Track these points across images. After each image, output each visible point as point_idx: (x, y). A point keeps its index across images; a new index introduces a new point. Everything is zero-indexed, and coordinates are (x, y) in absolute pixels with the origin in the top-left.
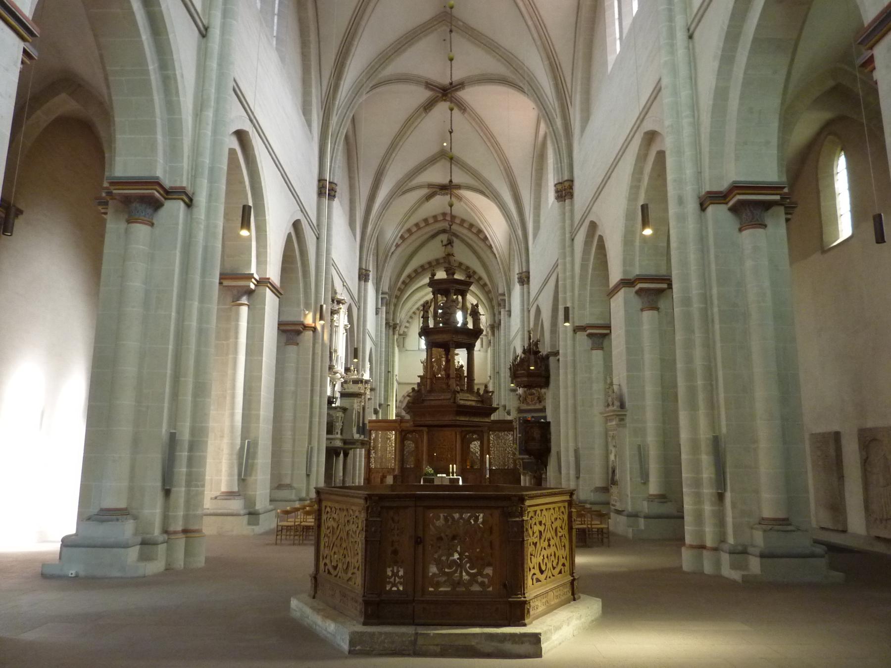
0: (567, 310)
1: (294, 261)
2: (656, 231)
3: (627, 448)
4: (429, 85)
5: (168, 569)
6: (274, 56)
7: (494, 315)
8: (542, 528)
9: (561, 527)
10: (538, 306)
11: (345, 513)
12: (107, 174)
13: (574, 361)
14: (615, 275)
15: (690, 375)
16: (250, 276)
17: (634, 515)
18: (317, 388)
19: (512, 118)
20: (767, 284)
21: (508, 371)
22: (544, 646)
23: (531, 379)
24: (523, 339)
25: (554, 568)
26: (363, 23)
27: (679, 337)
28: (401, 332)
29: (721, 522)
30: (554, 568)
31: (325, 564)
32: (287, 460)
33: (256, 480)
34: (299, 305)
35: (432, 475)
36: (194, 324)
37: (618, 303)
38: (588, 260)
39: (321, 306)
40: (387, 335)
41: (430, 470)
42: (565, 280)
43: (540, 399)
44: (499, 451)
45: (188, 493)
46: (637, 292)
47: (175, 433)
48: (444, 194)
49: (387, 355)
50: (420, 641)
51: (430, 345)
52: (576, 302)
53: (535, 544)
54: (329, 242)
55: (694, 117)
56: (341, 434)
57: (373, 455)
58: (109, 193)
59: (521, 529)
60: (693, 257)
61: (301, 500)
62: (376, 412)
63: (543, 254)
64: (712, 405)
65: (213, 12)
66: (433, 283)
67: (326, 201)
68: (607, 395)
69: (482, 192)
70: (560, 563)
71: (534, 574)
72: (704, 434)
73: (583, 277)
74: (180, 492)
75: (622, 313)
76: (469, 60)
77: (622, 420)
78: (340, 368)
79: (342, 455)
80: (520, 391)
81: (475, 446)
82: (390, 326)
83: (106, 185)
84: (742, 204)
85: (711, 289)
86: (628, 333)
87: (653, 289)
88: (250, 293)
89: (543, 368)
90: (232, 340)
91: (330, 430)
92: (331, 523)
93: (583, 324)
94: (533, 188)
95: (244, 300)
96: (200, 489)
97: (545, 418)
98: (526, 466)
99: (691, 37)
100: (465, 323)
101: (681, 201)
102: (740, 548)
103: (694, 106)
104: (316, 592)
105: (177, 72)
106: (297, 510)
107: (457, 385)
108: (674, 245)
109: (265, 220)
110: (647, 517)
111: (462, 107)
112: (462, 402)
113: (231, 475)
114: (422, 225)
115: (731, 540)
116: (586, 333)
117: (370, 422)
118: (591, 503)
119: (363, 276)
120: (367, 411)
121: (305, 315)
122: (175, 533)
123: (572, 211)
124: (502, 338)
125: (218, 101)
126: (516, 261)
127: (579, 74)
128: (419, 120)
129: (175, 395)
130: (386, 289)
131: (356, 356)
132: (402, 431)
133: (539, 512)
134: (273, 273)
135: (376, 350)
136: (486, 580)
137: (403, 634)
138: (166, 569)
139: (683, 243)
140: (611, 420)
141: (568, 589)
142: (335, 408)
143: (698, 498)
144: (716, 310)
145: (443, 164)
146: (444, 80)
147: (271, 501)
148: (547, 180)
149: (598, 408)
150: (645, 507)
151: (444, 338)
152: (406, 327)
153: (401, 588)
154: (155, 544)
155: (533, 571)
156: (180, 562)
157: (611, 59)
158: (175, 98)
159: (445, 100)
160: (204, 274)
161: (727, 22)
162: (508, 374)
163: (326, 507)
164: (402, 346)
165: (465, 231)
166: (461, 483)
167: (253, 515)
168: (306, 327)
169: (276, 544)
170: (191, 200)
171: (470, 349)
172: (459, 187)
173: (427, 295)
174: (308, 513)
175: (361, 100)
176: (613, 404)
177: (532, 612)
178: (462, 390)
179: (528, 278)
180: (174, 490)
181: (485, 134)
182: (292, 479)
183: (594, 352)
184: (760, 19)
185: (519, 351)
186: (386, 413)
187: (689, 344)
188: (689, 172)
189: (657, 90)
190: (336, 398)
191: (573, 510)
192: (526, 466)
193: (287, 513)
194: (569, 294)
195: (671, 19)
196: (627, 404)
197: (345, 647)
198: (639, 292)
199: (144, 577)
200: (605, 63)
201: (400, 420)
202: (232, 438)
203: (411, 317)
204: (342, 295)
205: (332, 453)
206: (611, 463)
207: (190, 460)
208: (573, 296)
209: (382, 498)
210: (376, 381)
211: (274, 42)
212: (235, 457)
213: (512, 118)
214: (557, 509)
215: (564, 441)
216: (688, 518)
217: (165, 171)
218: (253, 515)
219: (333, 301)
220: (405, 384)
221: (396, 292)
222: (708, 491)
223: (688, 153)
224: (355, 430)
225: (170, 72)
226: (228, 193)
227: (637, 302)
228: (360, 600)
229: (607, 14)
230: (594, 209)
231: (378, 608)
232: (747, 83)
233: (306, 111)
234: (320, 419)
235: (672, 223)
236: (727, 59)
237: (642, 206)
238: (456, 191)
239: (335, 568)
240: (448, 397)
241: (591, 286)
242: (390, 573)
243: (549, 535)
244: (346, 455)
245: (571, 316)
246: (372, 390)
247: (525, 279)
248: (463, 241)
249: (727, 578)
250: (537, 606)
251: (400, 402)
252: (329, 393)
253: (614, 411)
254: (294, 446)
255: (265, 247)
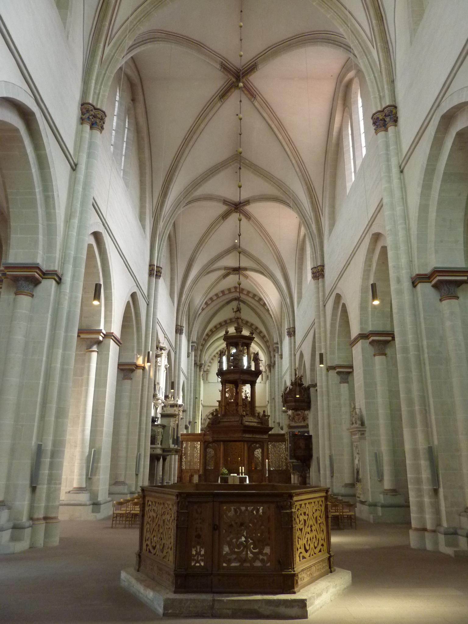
0: (321, 355)
1: (131, 320)
2: (382, 301)
3: (367, 453)
4: (225, 202)
5: (32, 547)
6: (121, 183)
7: (271, 357)
8: (306, 518)
9: (320, 517)
10: (301, 352)
11: (162, 506)
12: (3, 261)
13: (328, 392)
14: (355, 331)
15: (410, 403)
16: (99, 332)
17: (374, 505)
18: (145, 411)
19: (282, 224)
20: (461, 337)
21: (281, 398)
22: (310, 609)
23: (297, 404)
24: (291, 375)
25: (315, 548)
26: (182, 161)
27: (401, 375)
28: (205, 370)
29: (437, 512)
30: (315, 548)
31: (147, 545)
32: (122, 463)
33: (99, 479)
34: (133, 351)
35: (227, 474)
36: (59, 365)
37: (358, 350)
38: (336, 320)
39: (149, 353)
40: (195, 372)
41: (225, 471)
42: (320, 333)
43: (305, 419)
44: (276, 457)
45: (49, 489)
46: (370, 343)
47: (41, 445)
48: (236, 274)
49: (195, 386)
50: (217, 606)
51: (223, 383)
52: (328, 350)
53: (301, 530)
54: (155, 302)
55: (406, 224)
56: (161, 444)
57: (184, 460)
58: (4, 274)
59: (290, 518)
60: (409, 319)
61: (132, 493)
62: (186, 428)
63: (305, 315)
64: (426, 424)
65: (81, 154)
66: (227, 338)
67: (154, 279)
68: (351, 416)
69: (262, 273)
70: (320, 544)
71: (301, 553)
72: (422, 446)
73: (332, 332)
74: (43, 489)
75: (360, 357)
76: (252, 185)
77: (363, 434)
78: (161, 396)
79: (161, 459)
80: (290, 412)
81: (258, 453)
82: (197, 366)
83: (2, 268)
84: (441, 282)
85: (422, 341)
86: (365, 372)
87: (381, 341)
88: (99, 343)
89: (306, 396)
90: (85, 376)
91: (153, 442)
92: (152, 514)
93: (428, 270)
94: (296, 281)
95: (95, 348)
96: (58, 486)
97: (308, 432)
98: (295, 468)
99: (402, 172)
100: (249, 366)
101: (399, 281)
102: (452, 530)
103: (406, 217)
104: (139, 566)
105: (55, 193)
106: (128, 501)
107: (243, 411)
108: (395, 310)
109: (111, 292)
110: (383, 506)
111: (248, 217)
112: (247, 423)
113: (81, 475)
114: (221, 295)
115: (445, 524)
116: (336, 371)
117: (182, 435)
118: (342, 496)
119: (179, 330)
120: (180, 427)
121: (137, 358)
122: (38, 519)
123: (324, 286)
124: (276, 374)
125: (82, 213)
126: (286, 320)
127: (327, 194)
128: (218, 226)
129: (43, 416)
130: (195, 340)
131: (173, 388)
132: (205, 442)
133: (303, 505)
134: (116, 329)
135: (187, 383)
136: (265, 558)
137: (204, 600)
138: (30, 548)
139: (401, 309)
140: (355, 434)
141: (326, 564)
142: (157, 425)
143: (419, 491)
144: (426, 356)
145: (235, 254)
146: (236, 199)
147: (109, 494)
148: (306, 266)
149: (345, 425)
150: (381, 499)
151: (235, 378)
152: (209, 366)
153: (202, 564)
154: (23, 528)
155: (300, 551)
156: (40, 542)
157: (349, 185)
158: (52, 211)
159: (237, 212)
160: (66, 331)
161: (426, 162)
162: (281, 400)
163: (148, 501)
164: (206, 380)
165: (250, 299)
166: (248, 482)
167: (96, 505)
168: (137, 367)
169: (112, 527)
170: (60, 279)
171: (253, 385)
172: (246, 269)
173: (223, 345)
174: (136, 504)
175: (179, 212)
176: (356, 423)
177: (299, 583)
178: (247, 414)
179: (294, 332)
180: (38, 487)
181: (263, 234)
182: (125, 478)
183: (342, 385)
184: (447, 161)
185: (289, 384)
186: (194, 428)
187: (408, 381)
188: (404, 261)
189: (380, 207)
190: (158, 418)
191: (329, 503)
192: (295, 468)
193: (120, 504)
194: (323, 343)
195: (388, 160)
196: (366, 422)
197: (161, 611)
198: (372, 343)
199: (14, 554)
200: (345, 188)
201: (203, 435)
202: (83, 447)
203: (212, 359)
204: (164, 343)
205: (154, 458)
206: (356, 466)
207: (52, 465)
208: (326, 345)
209: (189, 495)
210: (187, 405)
211: (122, 174)
212: (84, 461)
213: (282, 224)
214: (317, 503)
215: (322, 449)
216: (413, 508)
217: (43, 260)
218: (96, 505)
219: (157, 348)
220: (208, 406)
221: (202, 341)
222: (426, 487)
223: (403, 247)
224: (171, 441)
225: (50, 194)
226: (86, 274)
227: (371, 350)
228: (172, 573)
229: (346, 156)
230: (338, 285)
231: (186, 580)
232: (440, 203)
233: (142, 218)
234: (146, 433)
235: (393, 296)
236: (427, 186)
237: (372, 285)
238: (244, 272)
239: (154, 548)
240: (238, 419)
241: (338, 338)
242: (194, 553)
243: (310, 522)
244: (164, 460)
245: (324, 359)
246: (183, 411)
247: (292, 333)
248: (249, 306)
249: (444, 554)
250: (303, 578)
251: (204, 420)
252: (153, 414)
253: (357, 428)
254: (127, 452)
255: (111, 311)
